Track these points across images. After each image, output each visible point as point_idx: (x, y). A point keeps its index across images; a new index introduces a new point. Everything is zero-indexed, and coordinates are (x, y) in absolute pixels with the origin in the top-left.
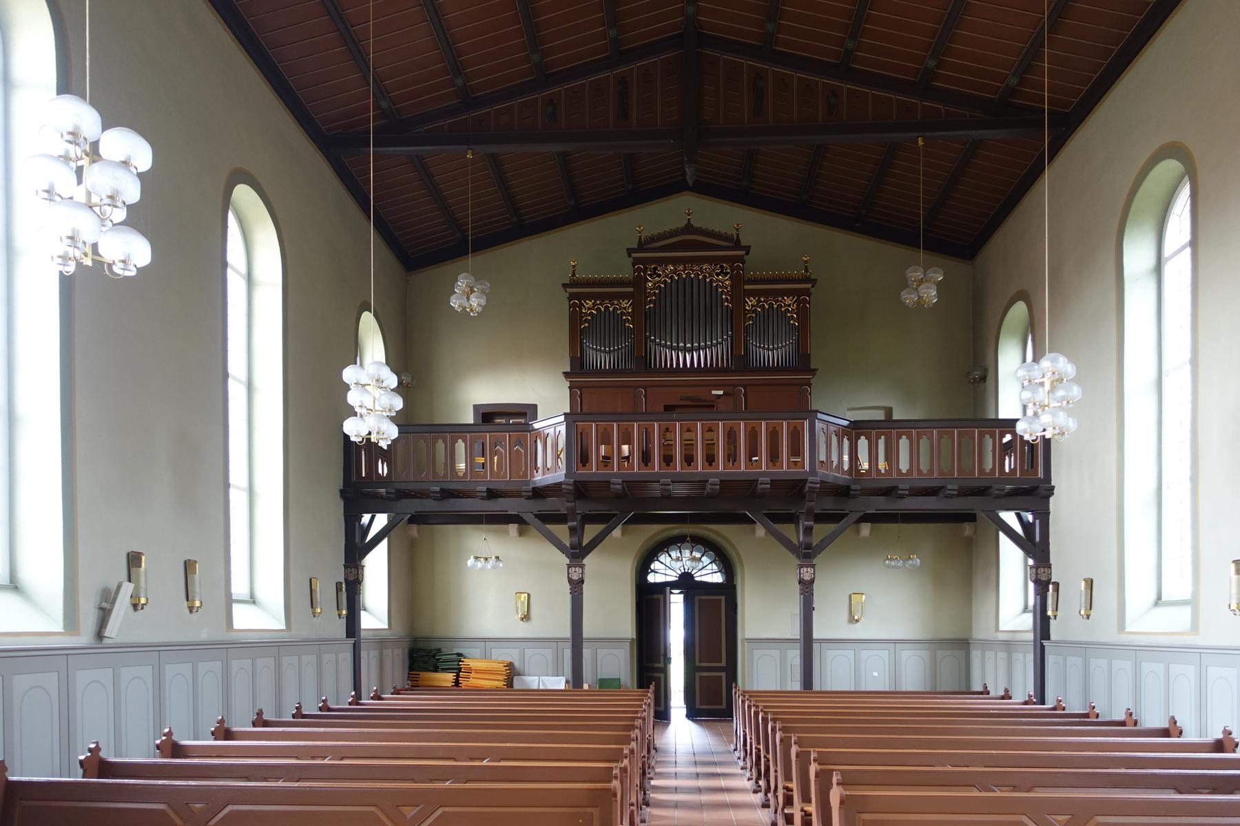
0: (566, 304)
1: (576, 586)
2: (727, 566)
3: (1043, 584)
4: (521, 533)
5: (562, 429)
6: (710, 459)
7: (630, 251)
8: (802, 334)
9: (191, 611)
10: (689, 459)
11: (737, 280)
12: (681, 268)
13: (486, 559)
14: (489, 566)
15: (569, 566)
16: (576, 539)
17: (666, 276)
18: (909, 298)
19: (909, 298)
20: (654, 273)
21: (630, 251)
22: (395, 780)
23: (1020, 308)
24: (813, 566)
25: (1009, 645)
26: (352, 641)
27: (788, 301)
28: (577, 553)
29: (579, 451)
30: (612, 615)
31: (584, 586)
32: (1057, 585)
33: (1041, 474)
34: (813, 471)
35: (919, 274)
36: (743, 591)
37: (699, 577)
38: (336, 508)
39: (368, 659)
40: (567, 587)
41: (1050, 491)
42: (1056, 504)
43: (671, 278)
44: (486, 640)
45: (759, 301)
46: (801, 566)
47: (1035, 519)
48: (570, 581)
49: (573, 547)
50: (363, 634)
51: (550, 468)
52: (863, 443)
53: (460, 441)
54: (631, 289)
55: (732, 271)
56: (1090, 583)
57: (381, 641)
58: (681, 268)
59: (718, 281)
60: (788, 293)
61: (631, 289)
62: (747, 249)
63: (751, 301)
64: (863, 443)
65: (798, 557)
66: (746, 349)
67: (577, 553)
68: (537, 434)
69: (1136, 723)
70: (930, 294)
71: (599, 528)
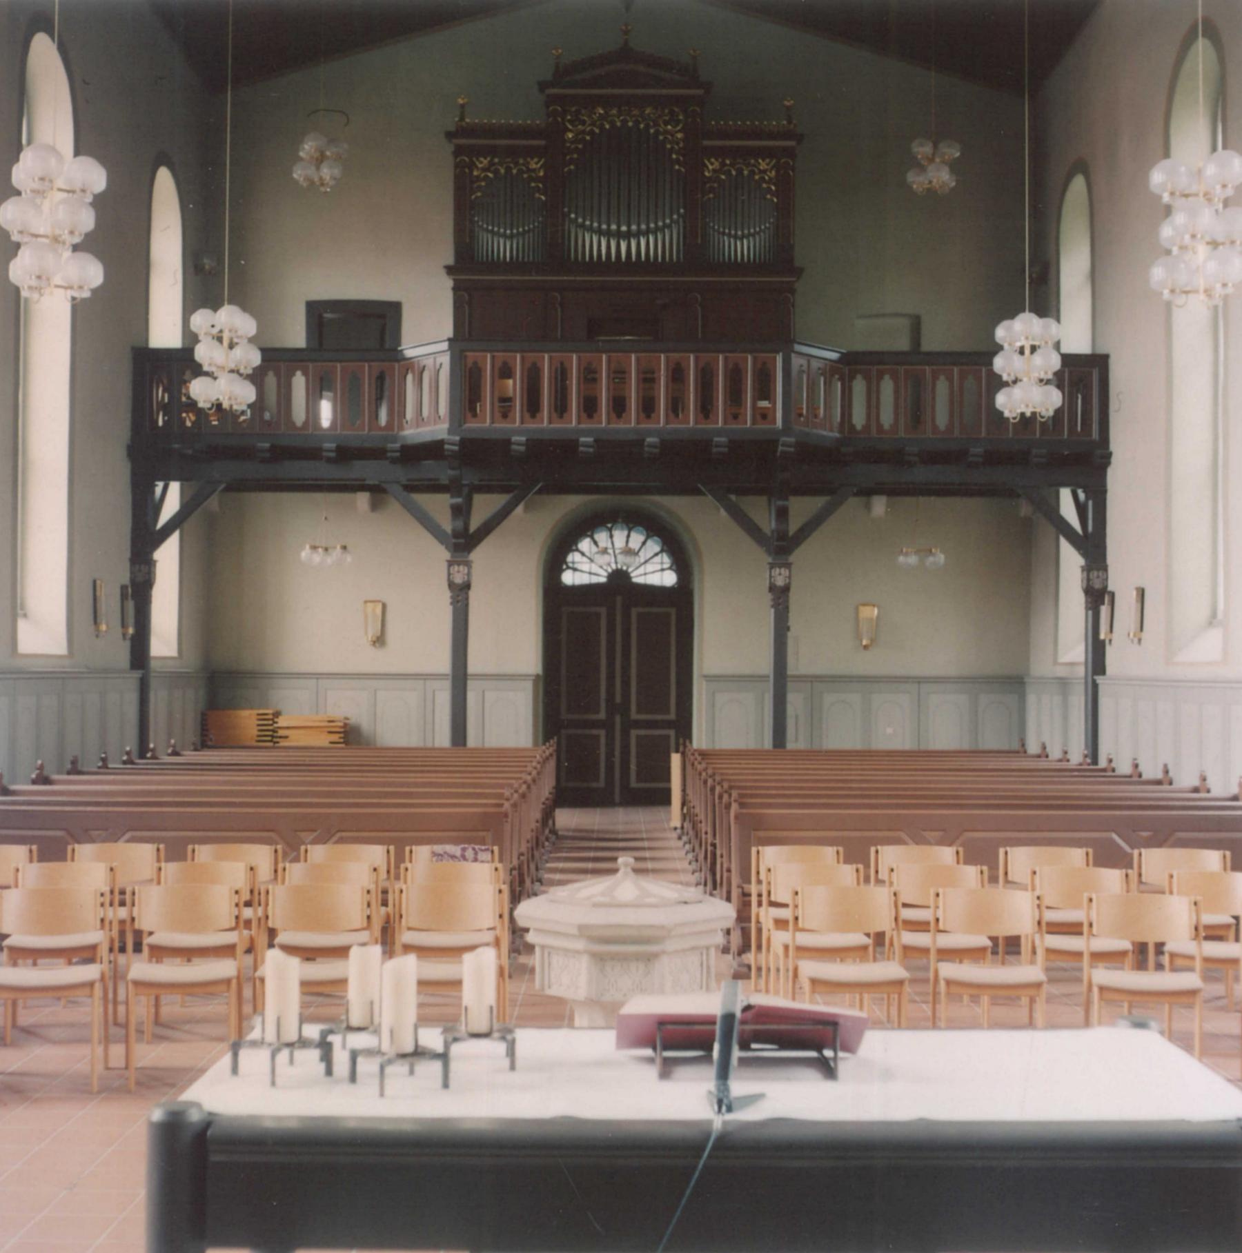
0: (450, 161)
1: (460, 593)
2: (682, 564)
3: (1097, 596)
4: (375, 506)
5: (445, 360)
6: (648, 407)
7: (542, 86)
8: (785, 210)
9: (97, 636)
10: (619, 406)
12: (614, 112)
13: (326, 549)
14: (329, 560)
15: (450, 564)
16: (460, 524)
17: (593, 124)
18: (917, 181)
19: (917, 181)
21: (542, 86)
23: (1078, 183)
24: (788, 566)
25: (1063, 684)
26: (137, 674)
27: (763, 165)
28: (463, 542)
29: (468, 389)
30: (511, 640)
31: (472, 594)
32: (1112, 595)
33: (1095, 435)
34: (787, 429)
35: (927, 149)
37: (638, 577)
38: (121, 470)
39: (158, 698)
41: (1107, 458)
42: (1116, 478)
44: (318, 676)
45: (723, 164)
46: (772, 566)
47: (1087, 498)
48: (451, 585)
49: (456, 534)
50: (154, 664)
51: (426, 412)
52: (859, 386)
53: (299, 373)
54: (543, 143)
56: (1141, 593)
57: (175, 679)
58: (614, 112)
59: (666, 132)
61: (543, 143)
63: (712, 165)
64: (859, 386)
65: (769, 552)
67: (463, 542)
68: (408, 365)
69: (1171, 783)
70: (941, 177)
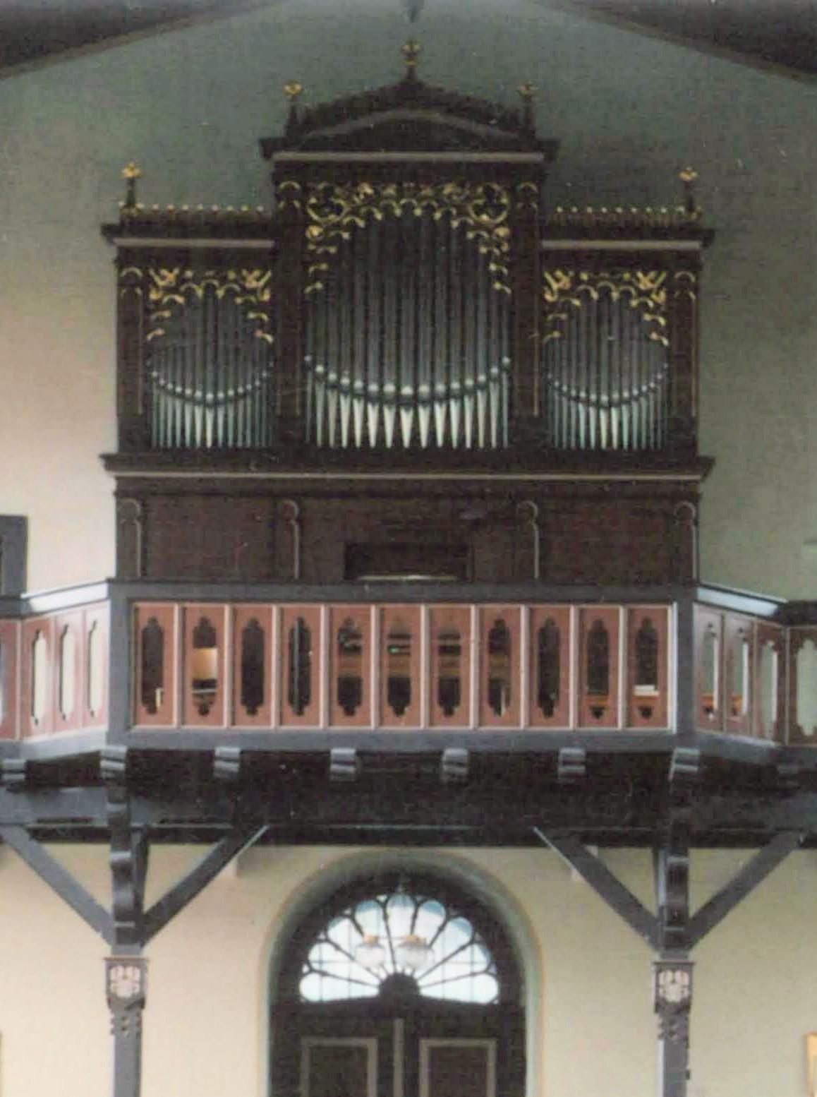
0: (110, 276)
1: (128, 1012)
2: (507, 963)
5: (102, 615)
6: (448, 696)
11: (527, 227)
15: (111, 964)
16: (127, 896)
17: (354, 212)
20: (327, 205)
22: (721, 678)
24: (688, 967)
27: (645, 282)
31: (147, 1015)
34: (685, 734)
36: (540, 1022)
37: (431, 988)
40: (105, 1017)
43: (369, 217)
45: (576, 281)
48: (112, 1000)
49: (120, 914)
54: (268, 244)
55: (514, 199)
58: (391, 191)
59: (479, 226)
60: (650, 262)
62: (550, 148)
63: (558, 282)
65: (654, 943)
66: (544, 404)
67: (135, 926)
71: (191, 856)
